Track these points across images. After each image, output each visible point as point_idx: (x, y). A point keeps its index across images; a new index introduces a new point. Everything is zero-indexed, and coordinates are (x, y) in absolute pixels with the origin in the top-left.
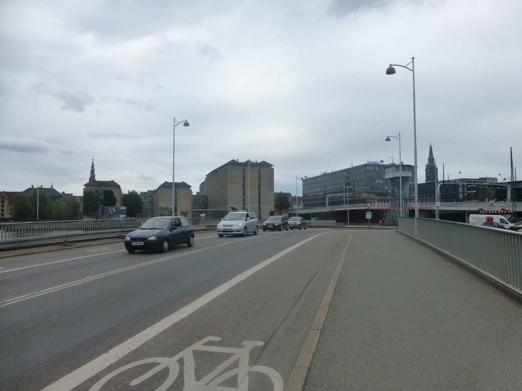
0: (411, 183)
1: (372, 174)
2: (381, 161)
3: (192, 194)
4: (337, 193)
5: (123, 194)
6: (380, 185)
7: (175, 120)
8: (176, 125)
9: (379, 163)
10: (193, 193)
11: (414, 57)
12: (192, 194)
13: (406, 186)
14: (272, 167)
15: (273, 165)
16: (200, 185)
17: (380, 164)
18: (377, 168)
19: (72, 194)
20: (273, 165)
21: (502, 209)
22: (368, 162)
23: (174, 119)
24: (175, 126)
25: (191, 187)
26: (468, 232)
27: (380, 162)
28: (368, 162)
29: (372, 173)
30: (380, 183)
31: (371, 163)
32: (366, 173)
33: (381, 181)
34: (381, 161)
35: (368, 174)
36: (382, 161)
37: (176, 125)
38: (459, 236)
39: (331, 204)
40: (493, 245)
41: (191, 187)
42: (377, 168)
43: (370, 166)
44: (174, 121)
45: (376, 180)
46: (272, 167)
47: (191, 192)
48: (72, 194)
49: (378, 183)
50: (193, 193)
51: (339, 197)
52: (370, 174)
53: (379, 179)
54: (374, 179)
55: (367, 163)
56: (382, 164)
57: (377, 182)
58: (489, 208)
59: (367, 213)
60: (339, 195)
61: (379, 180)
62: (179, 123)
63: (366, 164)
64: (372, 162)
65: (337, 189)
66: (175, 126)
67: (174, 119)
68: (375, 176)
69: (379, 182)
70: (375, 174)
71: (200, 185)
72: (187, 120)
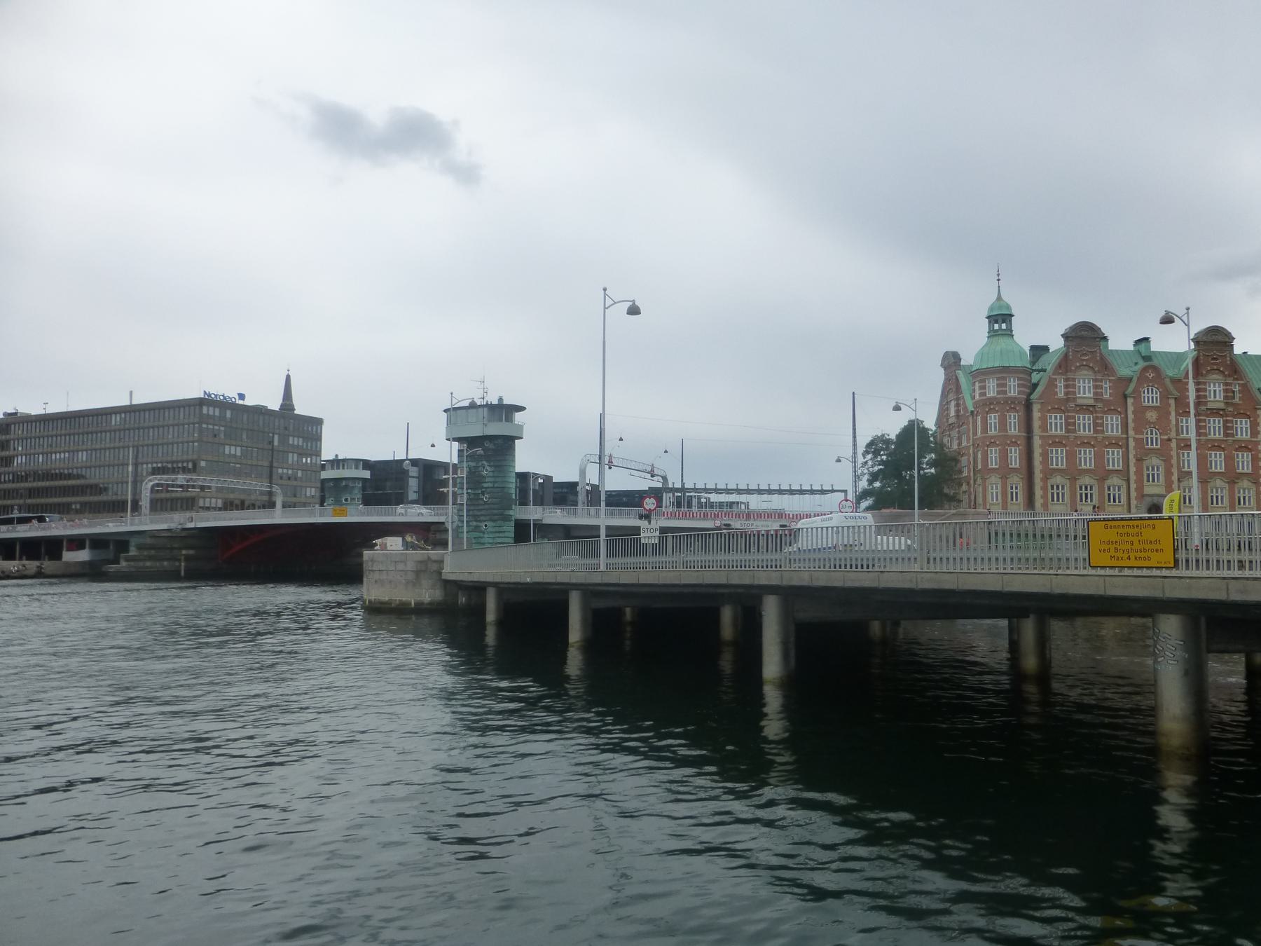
0: (307, 460)
1: (216, 427)
2: (239, 394)
4: (174, 471)
6: (233, 460)
8: (609, 307)
9: (233, 400)
11: (952, 348)
17: (237, 402)
18: (229, 414)
19: (318, 422)
22: (205, 392)
23: (605, 290)
24: (606, 306)
26: (698, 541)
27: (237, 398)
28: (205, 392)
29: (216, 425)
30: (235, 456)
31: (213, 396)
32: (200, 423)
33: (239, 449)
34: (239, 394)
35: (204, 426)
36: (242, 396)
37: (609, 307)
38: (696, 543)
39: (159, 505)
40: (835, 535)
42: (229, 414)
43: (211, 406)
44: (605, 294)
45: (224, 445)
49: (230, 455)
51: (181, 486)
52: (211, 427)
53: (233, 445)
54: (221, 444)
55: (203, 397)
56: (241, 402)
57: (227, 452)
60: (181, 479)
61: (233, 448)
62: (615, 303)
63: (201, 399)
64: (216, 396)
65: (79, 465)
66: (606, 306)
67: (605, 290)
68: (222, 436)
69: (233, 452)
70: (222, 429)
72: (634, 301)
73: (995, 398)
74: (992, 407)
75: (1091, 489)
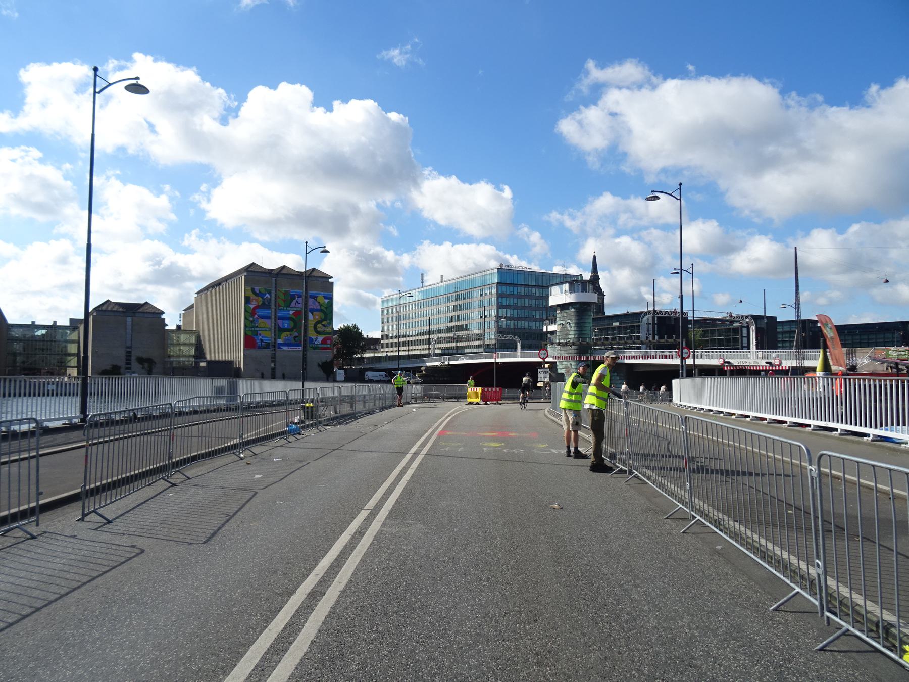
3: (167, 328)
5: (337, 325)
7: (98, 73)
10: (167, 325)
12: (167, 328)
13: (588, 319)
14: (331, 280)
15: (332, 277)
16: (196, 295)
19: (776, 317)
20: (332, 277)
21: (767, 363)
24: (98, 90)
25: (163, 313)
41: (163, 313)
44: (96, 75)
46: (331, 280)
47: (163, 323)
48: (776, 317)
50: (167, 325)
58: (742, 360)
59: (539, 370)
71: (196, 295)
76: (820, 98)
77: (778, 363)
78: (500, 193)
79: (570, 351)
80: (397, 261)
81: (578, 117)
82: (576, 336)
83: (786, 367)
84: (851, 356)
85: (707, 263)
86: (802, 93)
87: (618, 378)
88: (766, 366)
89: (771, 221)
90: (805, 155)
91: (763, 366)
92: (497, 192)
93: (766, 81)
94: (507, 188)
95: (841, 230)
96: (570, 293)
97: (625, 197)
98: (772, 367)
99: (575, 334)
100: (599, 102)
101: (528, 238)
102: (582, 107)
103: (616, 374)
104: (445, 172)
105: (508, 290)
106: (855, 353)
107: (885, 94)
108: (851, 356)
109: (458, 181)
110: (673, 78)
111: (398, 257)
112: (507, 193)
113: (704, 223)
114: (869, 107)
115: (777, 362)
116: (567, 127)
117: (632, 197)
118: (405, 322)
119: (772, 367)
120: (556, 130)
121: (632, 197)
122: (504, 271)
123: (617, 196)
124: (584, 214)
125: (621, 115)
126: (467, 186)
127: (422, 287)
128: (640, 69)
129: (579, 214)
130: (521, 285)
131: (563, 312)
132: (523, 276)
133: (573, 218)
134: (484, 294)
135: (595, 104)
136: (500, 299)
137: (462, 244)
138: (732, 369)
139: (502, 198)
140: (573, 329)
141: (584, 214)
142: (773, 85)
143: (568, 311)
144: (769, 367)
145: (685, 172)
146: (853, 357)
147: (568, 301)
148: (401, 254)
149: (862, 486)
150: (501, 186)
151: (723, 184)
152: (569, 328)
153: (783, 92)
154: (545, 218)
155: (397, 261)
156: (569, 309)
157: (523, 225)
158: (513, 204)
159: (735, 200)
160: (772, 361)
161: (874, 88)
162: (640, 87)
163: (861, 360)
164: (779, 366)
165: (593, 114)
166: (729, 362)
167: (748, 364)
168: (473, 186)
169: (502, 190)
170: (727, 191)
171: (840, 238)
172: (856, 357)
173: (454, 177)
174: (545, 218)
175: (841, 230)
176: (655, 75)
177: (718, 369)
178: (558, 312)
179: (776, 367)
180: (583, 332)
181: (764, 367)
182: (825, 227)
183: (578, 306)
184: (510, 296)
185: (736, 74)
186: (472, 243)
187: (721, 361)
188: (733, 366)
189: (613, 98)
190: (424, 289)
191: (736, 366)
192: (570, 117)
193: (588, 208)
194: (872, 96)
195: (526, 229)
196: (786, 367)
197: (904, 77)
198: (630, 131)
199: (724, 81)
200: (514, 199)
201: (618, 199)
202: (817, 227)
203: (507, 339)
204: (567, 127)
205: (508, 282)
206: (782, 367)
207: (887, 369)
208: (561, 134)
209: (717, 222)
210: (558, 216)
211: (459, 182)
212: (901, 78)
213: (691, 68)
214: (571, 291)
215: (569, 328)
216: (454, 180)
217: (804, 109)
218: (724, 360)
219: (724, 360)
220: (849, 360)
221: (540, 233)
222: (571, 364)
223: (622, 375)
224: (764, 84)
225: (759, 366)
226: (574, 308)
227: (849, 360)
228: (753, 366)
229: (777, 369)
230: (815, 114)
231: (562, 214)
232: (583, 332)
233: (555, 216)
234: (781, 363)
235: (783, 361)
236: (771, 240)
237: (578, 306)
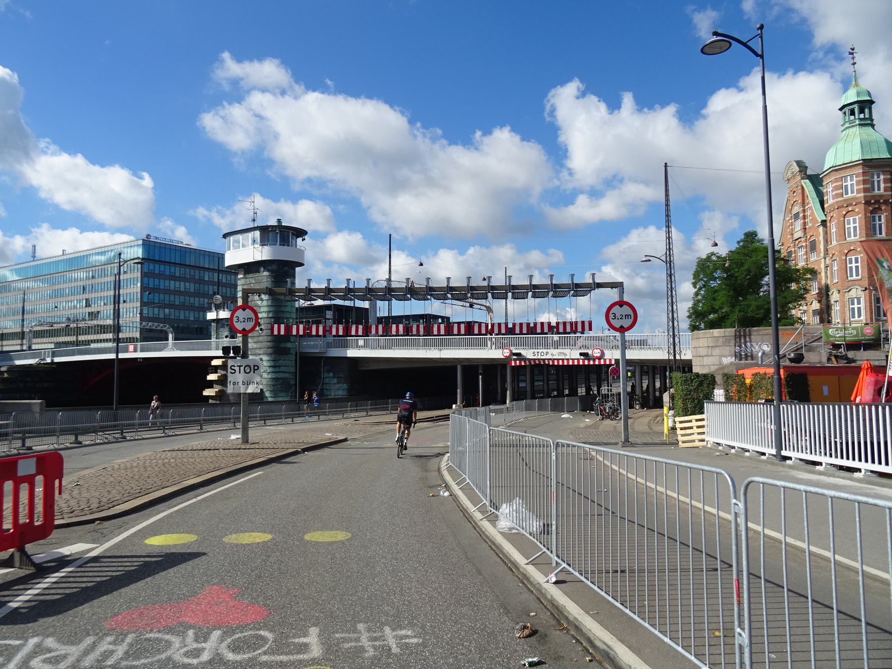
21: (581, 354)
48: (623, 283)
73: (854, 198)
74: (850, 209)
75: (859, 303)
76: (439, 132)
77: (598, 355)
78: (140, 181)
79: (261, 338)
80: (6, 243)
81: (222, 113)
82: (271, 315)
83: (610, 360)
84: (743, 341)
85: (353, 272)
86: (425, 126)
87: (335, 381)
88: (578, 360)
89: (406, 238)
90: (431, 182)
91: (573, 360)
92: (135, 179)
93: (397, 108)
94: (146, 175)
95: (462, 252)
96: (263, 245)
97: (276, 200)
98: (589, 360)
99: (269, 312)
100: (242, 103)
101: (173, 232)
102: (225, 104)
103: (331, 374)
104: (69, 148)
105: (157, 268)
106: (750, 335)
107: (486, 139)
108: (743, 341)
109: (87, 162)
110: (314, 90)
111: (7, 239)
112: (147, 182)
113: (349, 235)
114: (476, 149)
115: (597, 353)
116: (210, 121)
117: (282, 200)
118: (30, 316)
119: (589, 360)
120: (198, 124)
121: (282, 200)
122: (151, 244)
123: (268, 198)
124: (233, 213)
125: (268, 120)
126: (96, 169)
127: (34, 261)
128: (283, 71)
129: (228, 212)
130: (175, 263)
131: (248, 276)
132: (178, 254)
133: (223, 216)
134: (128, 301)
135: (239, 102)
136: (146, 279)
137: (93, 232)
138: (523, 364)
139: (142, 187)
140: (265, 303)
141: (233, 213)
142: (402, 113)
143: (257, 274)
144: (584, 360)
145: (330, 185)
146: (745, 342)
147: (259, 258)
148: (12, 236)
149: (812, 555)
150: (139, 172)
151: (364, 201)
152: (259, 303)
153: (411, 122)
154: (191, 212)
155: (6, 243)
156: (259, 272)
157: (166, 218)
158: (154, 193)
159: (376, 216)
160: (590, 352)
161: (478, 134)
162: (283, 93)
163: (760, 347)
164: (599, 359)
165: (237, 112)
166: (519, 355)
167: (549, 357)
168: (105, 170)
169: (141, 178)
170: (369, 208)
171: (461, 258)
172: (751, 342)
173: (80, 155)
174: (191, 212)
175: (462, 252)
176: (296, 82)
177: (483, 365)
178: (240, 276)
179: (594, 360)
180: (283, 309)
181: (561, 361)
182: (450, 248)
183: (274, 267)
184: (161, 276)
185: (370, 97)
186: (106, 231)
187: (507, 353)
188: (525, 359)
189: (257, 99)
190: (36, 263)
191: (530, 360)
192: (213, 112)
193: (237, 207)
194: (478, 141)
195: (169, 223)
196: (610, 360)
197: (499, 127)
198: (276, 136)
199: (360, 101)
200: (155, 188)
201: (267, 201)
202: (443, 248)
203: (156, 324)
204: (210, 121)
205: (156, 258)
206: (605, 360)
207: (829, 360)
208: (204, 128)
209: (362, 234)
210: (206, 213)
211: (89, 163)
212: (496, 128)
213: (329, 83)
214: (263, 244)
215: (259, 303)
216: (80, 160)
217: (428, 141)
218: (511, 351)
219: (511, 351)
220: (740, 346)
221: (186, 228)
222: (261, 359)
223: (342, 375)
224: (395, 111)
225: (568, 360)
226: (268, 271)
227: (740, 346)
228: (558, 360)
229: (597, 363)
230: (436, 147)
231: (210, 211)
232: (283, 309)
233: (201, 212)
234: (603, 354)
235: (606, 352)
236: (408, 256)
237: (274, 267)
